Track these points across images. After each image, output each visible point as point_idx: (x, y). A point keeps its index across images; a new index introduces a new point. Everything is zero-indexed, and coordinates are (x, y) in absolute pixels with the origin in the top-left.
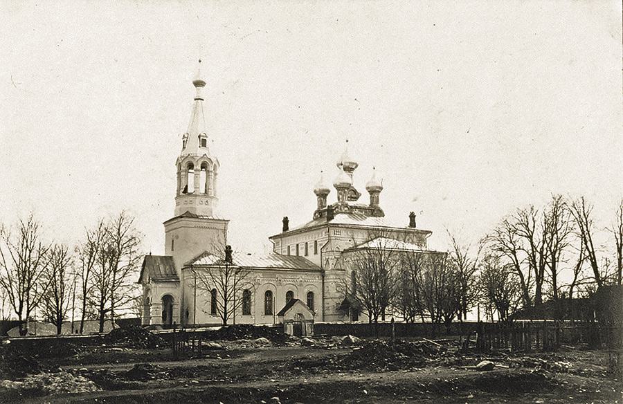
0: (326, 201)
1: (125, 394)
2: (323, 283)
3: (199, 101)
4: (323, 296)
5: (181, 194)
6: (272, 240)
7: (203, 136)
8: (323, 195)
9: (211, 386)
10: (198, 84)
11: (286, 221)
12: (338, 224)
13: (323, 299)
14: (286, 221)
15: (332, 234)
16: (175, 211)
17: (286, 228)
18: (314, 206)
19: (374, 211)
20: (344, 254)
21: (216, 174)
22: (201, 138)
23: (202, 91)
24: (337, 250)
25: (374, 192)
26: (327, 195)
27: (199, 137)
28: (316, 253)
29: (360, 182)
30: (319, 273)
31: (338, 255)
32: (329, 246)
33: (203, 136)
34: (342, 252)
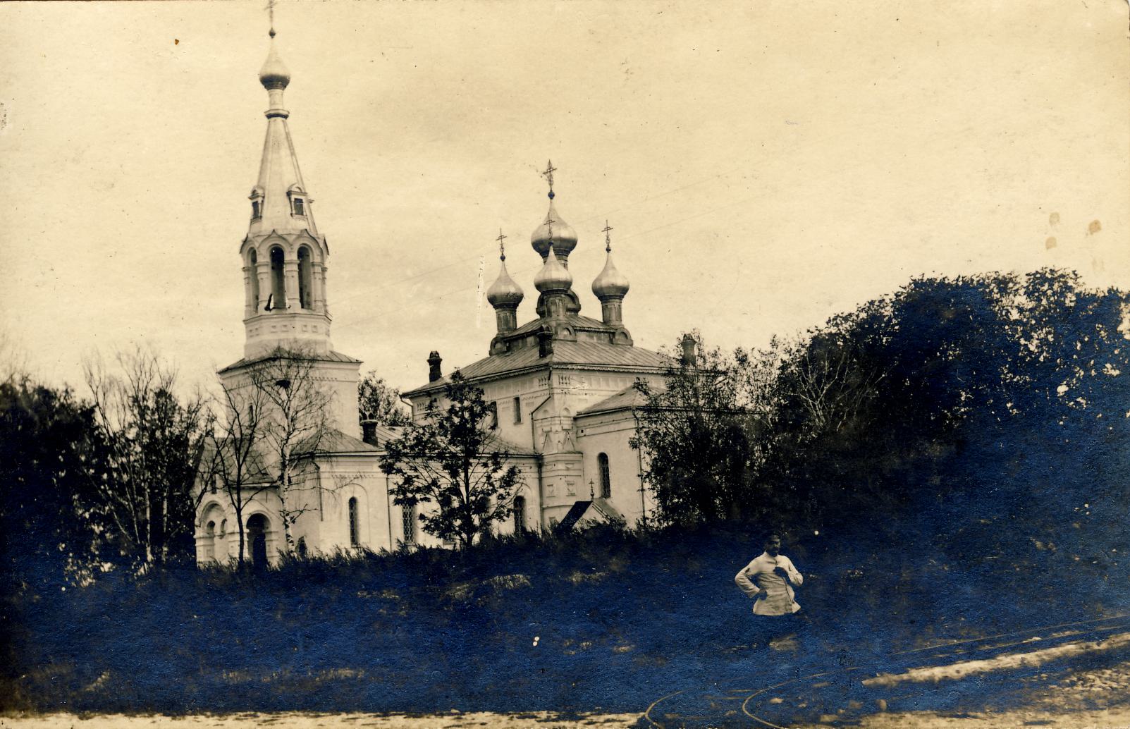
0: (515, 318)
1: (1019, 657)
2: (540, 479)
3: (279, 119)
4: (541, 505)
5: (261, 311)
6: (408, 401)
7: (296, 193)
8: (506, 304)
9: (233, 677)
10: (272, 82)
11: (435, 361)
12: (565, 364)
13: (543, 510)
14: (435, 361)
15: (555, 384)
16: (246, 347)
17: (435, 373)
18: (490, 329)
19: (612, 333)
20: (581, 423)
21: (324, 270)
22: (293, 197)
23: (285, 99)
24: (565, 413)
25: (610, 295)
26: (516, 305)
27: (289, 194)
28: (519, 420)
29: (581, 273)
30: (532, 461)
31: (567, 424)
32: (548, 408)
33: (296, 193)
34: (575, 419)
